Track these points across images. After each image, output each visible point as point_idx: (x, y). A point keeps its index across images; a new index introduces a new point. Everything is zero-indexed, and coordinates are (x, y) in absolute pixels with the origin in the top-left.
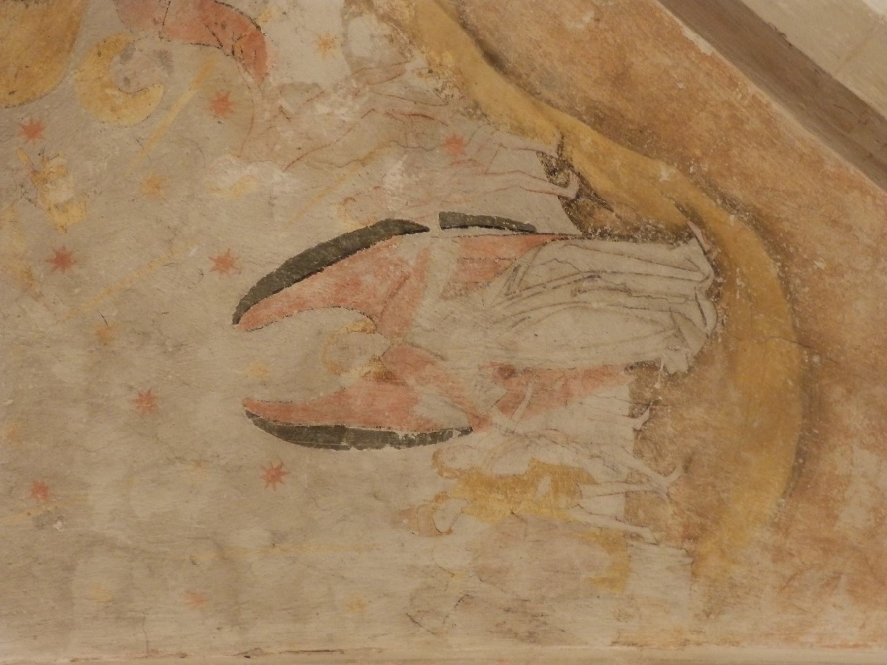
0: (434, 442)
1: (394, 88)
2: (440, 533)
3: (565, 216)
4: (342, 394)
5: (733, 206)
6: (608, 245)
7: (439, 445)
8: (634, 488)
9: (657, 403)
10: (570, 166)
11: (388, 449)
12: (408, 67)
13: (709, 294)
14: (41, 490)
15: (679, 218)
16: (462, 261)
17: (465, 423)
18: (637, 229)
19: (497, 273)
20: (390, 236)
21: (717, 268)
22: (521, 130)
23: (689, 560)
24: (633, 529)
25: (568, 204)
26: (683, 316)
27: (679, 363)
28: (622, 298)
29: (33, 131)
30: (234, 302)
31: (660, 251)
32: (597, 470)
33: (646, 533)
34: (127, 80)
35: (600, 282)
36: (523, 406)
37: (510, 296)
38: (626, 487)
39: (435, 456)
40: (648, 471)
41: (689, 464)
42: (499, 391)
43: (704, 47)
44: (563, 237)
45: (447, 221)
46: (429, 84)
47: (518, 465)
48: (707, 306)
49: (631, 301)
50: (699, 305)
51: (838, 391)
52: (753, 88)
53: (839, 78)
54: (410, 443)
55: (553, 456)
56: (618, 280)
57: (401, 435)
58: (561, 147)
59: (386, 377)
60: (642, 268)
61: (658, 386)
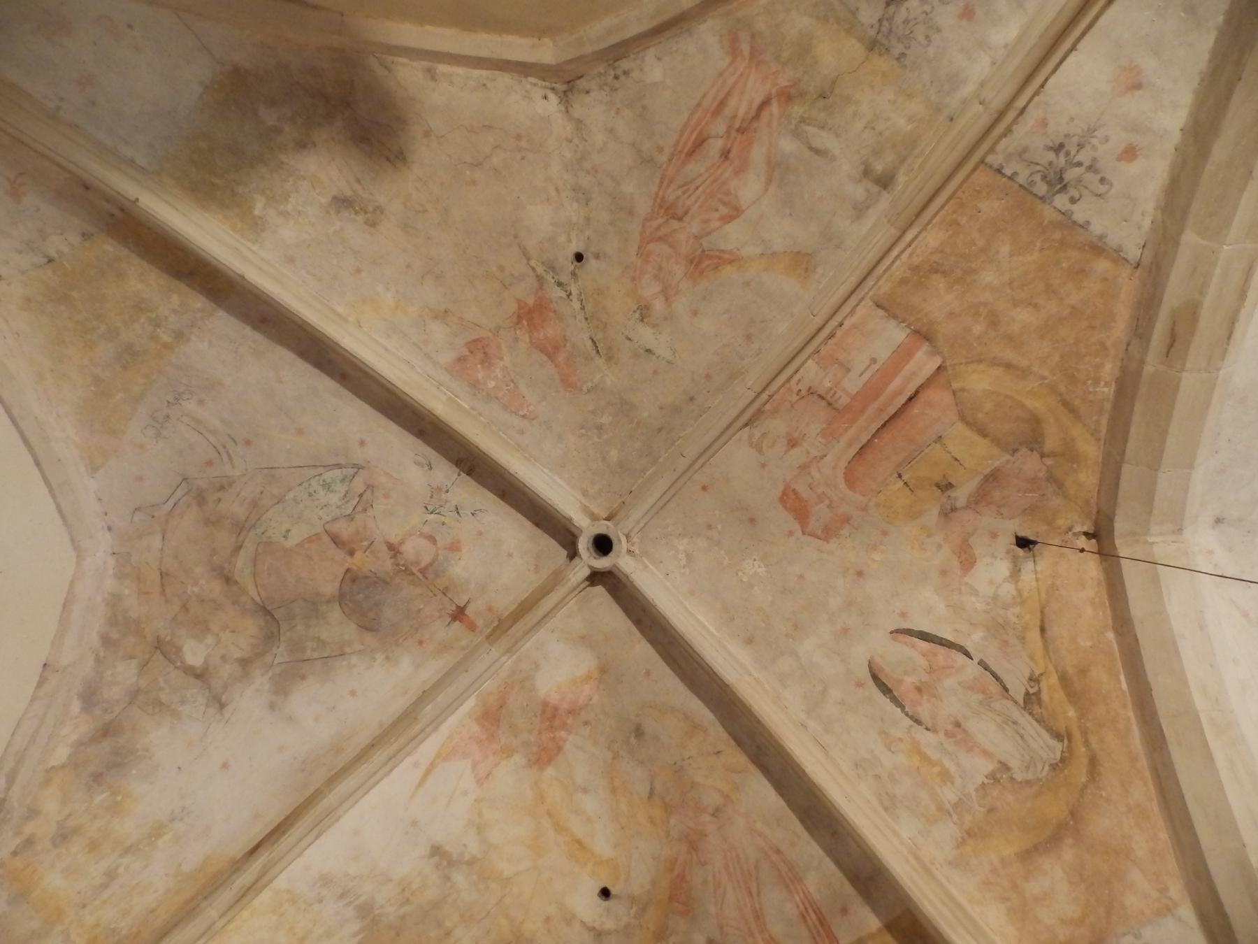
0: (915, 722)
1: (1001, 612)
2: (890, 750)
3: (1022, 696)
4: (900, 681)
5: (1088, 746)
6: (1029, 718)
7: (915, 724)
8: (965, 799)
9: (999, 781)
10: (1039, 683)
11: (899, 710)
12: (1011, 609)
13: (1051, 765)
14: (796, 627)
15: (1063, 731)
16: (975, 679)
17: (930, 726)
18: (1044, 722)
19: (983, 692)
20: (959, 651)
21: (1062, 760)
22: (1032, 658)
23: (960, 840)
24: (951, 810)
25: (1027, 694)
26: (1035, 763)
27: (1019, 776)
28: (1018, 739)
29: (885, 533)
30: (896, 628)
31: (1046, 736)
32: (958, 781)
33: (955, 817)
34: (923, 544)
35: (1015, 726)
36: (954, 739)
37: (981, 703)
38: (963, 797)
39: (911, 726)
40: (974, 798)
41: (991, 810)
42: (950, 727)
43: (1124, 686)
44: (1016, 702)
45: (981, 663)
46: (1013, 619)
47: (934, 755)
48: (1047, 768)
49: (1020, 742)
50: (1044, 765)
51: (1069, 841)
52: (1131, 714)
53: (1162, 720)
54: (907, 715)
55: (948, 764)
56: (1022, 732)
57: (907, 710)
58: (1041, 674)
59: (919, 689)
60: (1035, 735)
61: (1004, 776)
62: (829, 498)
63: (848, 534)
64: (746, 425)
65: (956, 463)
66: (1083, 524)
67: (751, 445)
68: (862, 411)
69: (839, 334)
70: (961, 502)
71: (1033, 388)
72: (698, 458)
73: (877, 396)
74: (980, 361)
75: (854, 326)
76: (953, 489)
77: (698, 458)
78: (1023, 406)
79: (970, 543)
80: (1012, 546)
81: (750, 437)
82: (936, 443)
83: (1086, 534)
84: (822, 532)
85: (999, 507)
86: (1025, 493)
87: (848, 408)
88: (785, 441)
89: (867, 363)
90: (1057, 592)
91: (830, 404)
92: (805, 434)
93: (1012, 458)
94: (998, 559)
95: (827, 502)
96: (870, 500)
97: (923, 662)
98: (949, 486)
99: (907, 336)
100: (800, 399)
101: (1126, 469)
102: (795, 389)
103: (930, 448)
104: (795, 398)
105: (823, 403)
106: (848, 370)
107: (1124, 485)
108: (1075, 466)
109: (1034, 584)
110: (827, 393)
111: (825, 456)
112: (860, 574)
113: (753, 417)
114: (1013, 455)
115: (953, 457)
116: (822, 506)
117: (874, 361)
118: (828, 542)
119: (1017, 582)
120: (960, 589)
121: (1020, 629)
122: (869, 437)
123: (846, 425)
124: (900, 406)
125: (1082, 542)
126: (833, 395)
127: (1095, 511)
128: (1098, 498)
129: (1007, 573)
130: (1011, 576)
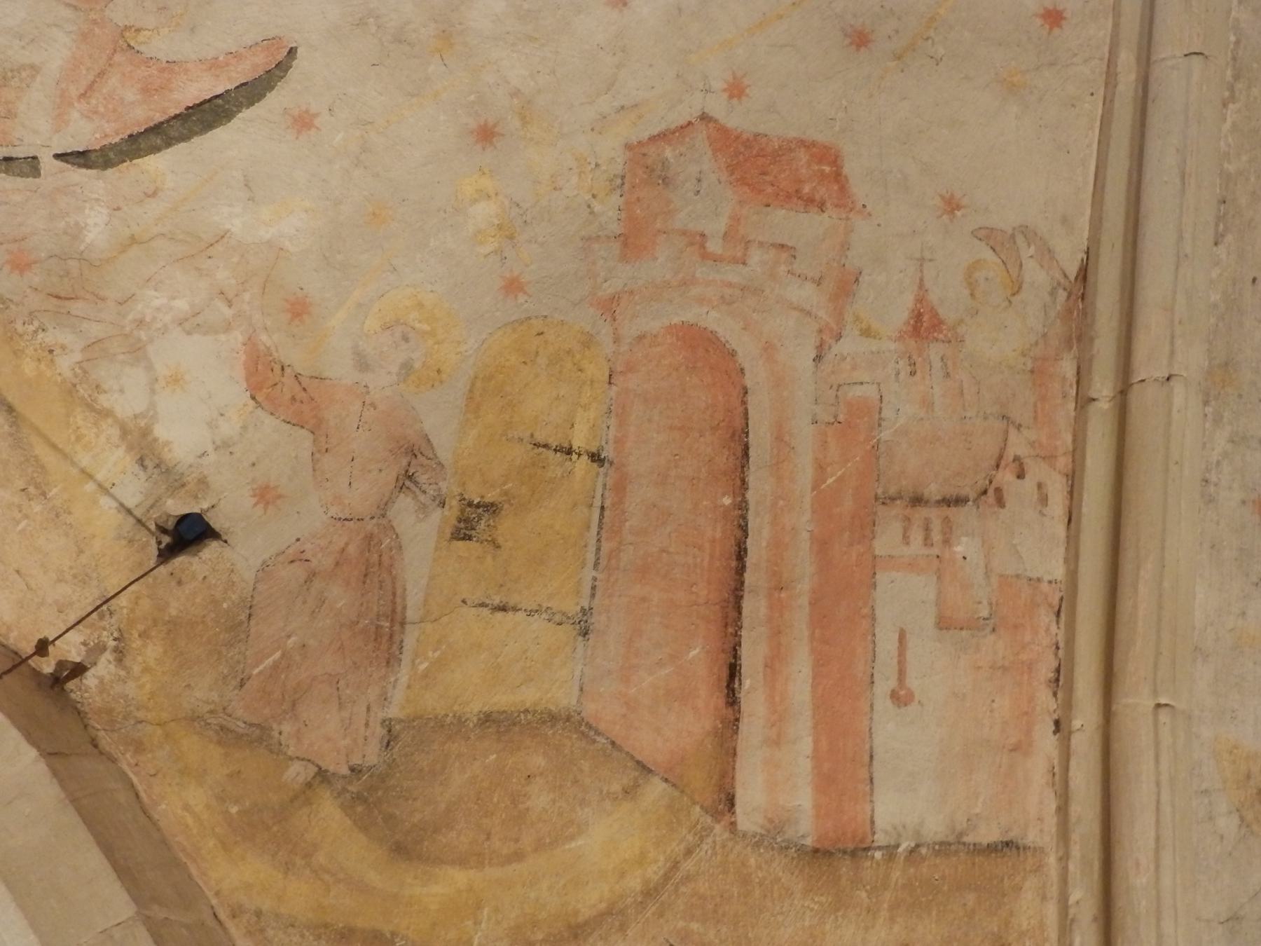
1: (96, 330)
12: (78, 357)
20: (103, 149)
29: (513, 286)
62: (717, 259)
63: (597, 207)
64: (1084, 274)
65: (497, 600)
66: (102, 687)
67: (1026, 232)
68: (822, 546)
69: (1046, 701)
70: (404, 511)
71: (477, 923)
72: (1144, 82)
73: (821, 617)
74: (650, 893)
75: (1021, 748)
76: (448, 531)
77: (1144, 82)
78: (462, 862)
79: (304, 432)
80: (205, 506)
81: (1047, 254)
82: (583, 611)
83: (78, 670)
84: (664, 163)
85: (312, 576)
86: (283, 655)
87: (865, 527)
88: (948, 314)
89: (913, 682)
90: (20, 484)
91: (918, 501)
92: (913, 373)
93: (381, 715)
94: (210, 449)
95: (714, 246)
96: (617, 340)
97: (160, 46)
98: (463, 531)
99: (873, 822)
100: (1001, 457)
101: (120, 905)
102: (1036, 471)
103: (587, 590)
104: (1018, 446)
105: (933, 490)
106: (944, 624)
107: (93, 860)
108: (234, 810)
109: (85, 460)
110: (946, 520)
111: (818, 358)
112: (487, 135)
113: (1084, 313)
114: (388, 724)
115: (515, 609)
116: (716, 226)
117: (901, 698)
118: (628, 147)
119: (125, 432)
120: (230, 304)
121: (20, 328)
122: (750, 495)
123: (830, 481)
124: (743, 633)
125: (71, 648)
126: (927, 529)
127: (105, 740)
128: (124, 776)
129: (160, 432)
130: (145, 433)
